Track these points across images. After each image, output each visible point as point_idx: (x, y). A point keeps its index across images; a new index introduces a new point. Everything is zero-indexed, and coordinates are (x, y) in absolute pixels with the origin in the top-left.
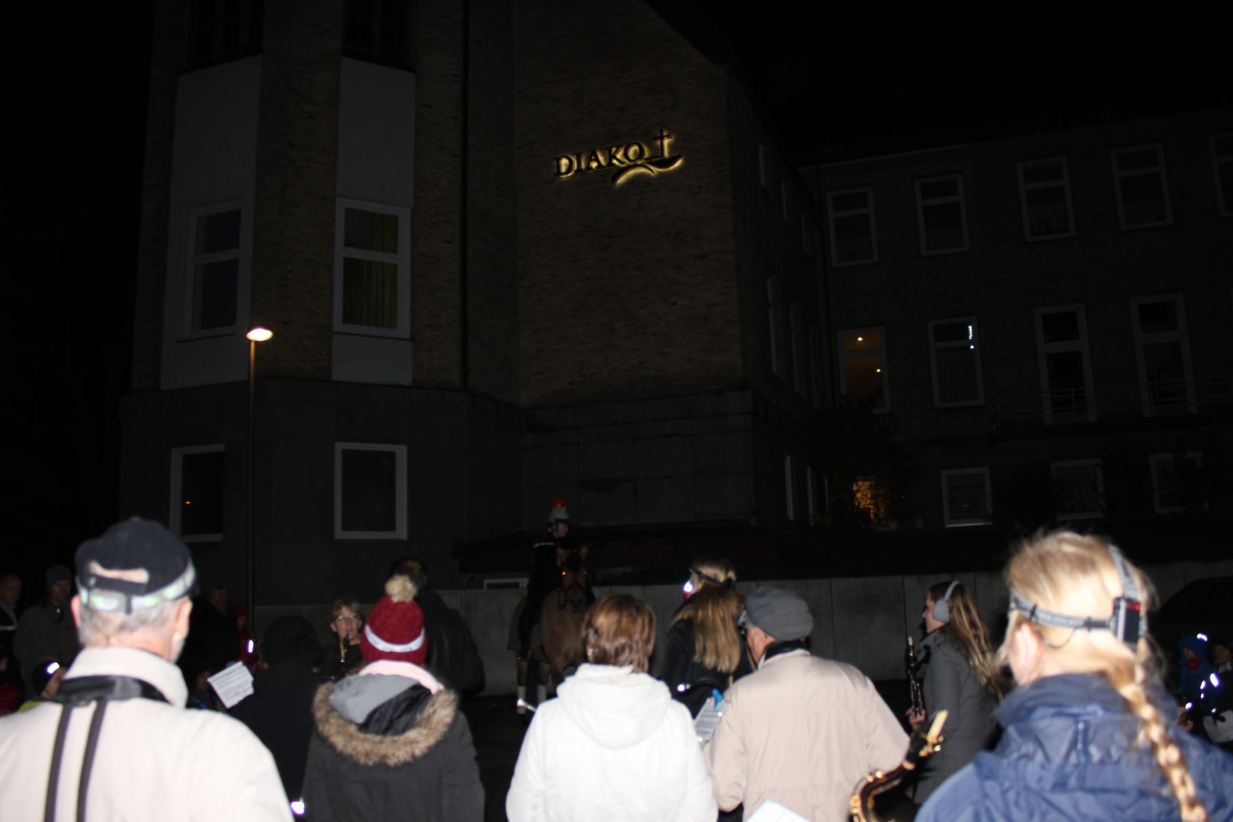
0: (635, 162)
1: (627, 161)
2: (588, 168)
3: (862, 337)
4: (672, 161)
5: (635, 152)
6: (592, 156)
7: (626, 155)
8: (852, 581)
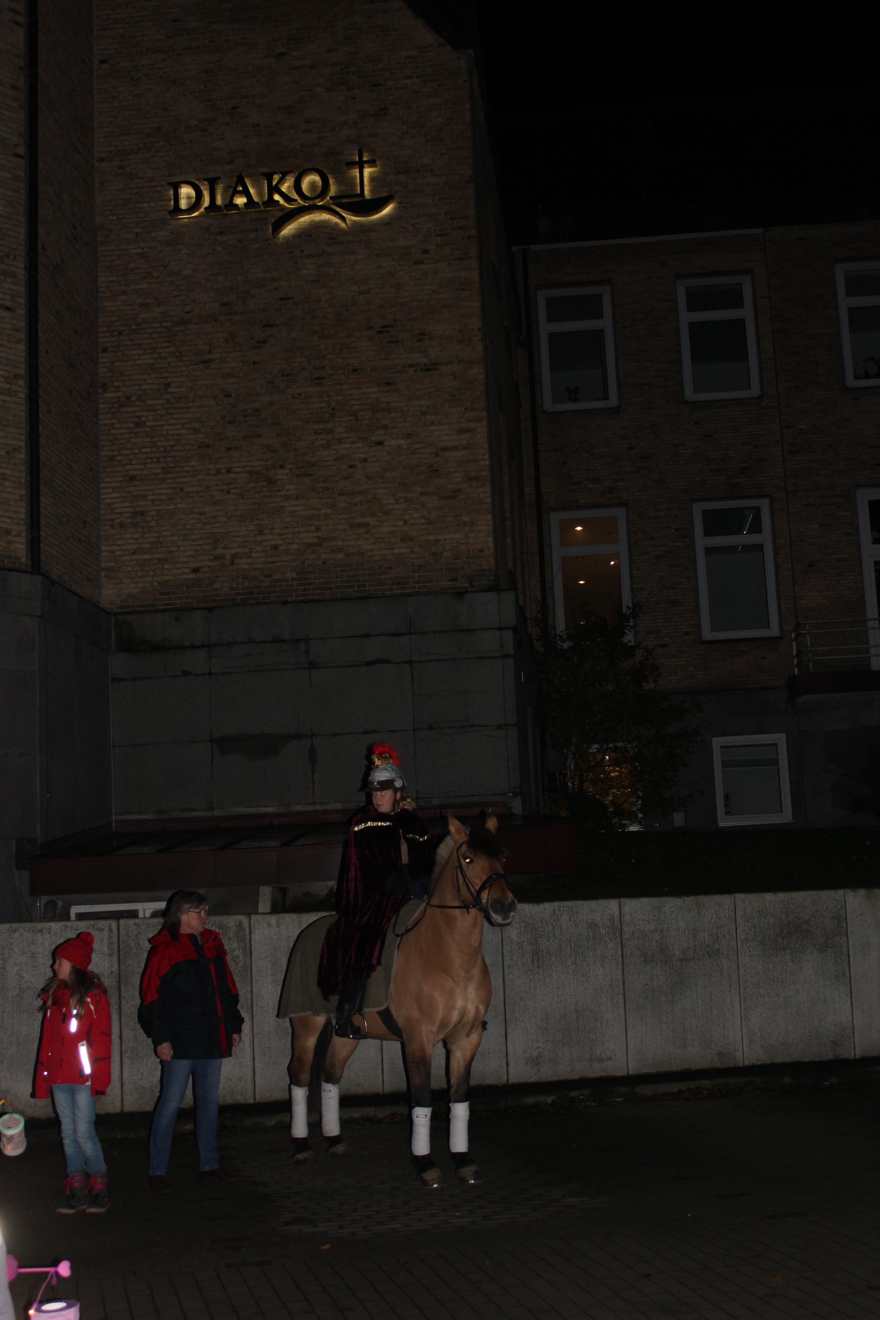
0: (311, 202)
1: (295, 196)
2: (231, 205)
3: (46, 1075)
4: (377, 204)
5: (313, 185)
6: (238, 185)
7: (297, 187)
8: (769, 897)
